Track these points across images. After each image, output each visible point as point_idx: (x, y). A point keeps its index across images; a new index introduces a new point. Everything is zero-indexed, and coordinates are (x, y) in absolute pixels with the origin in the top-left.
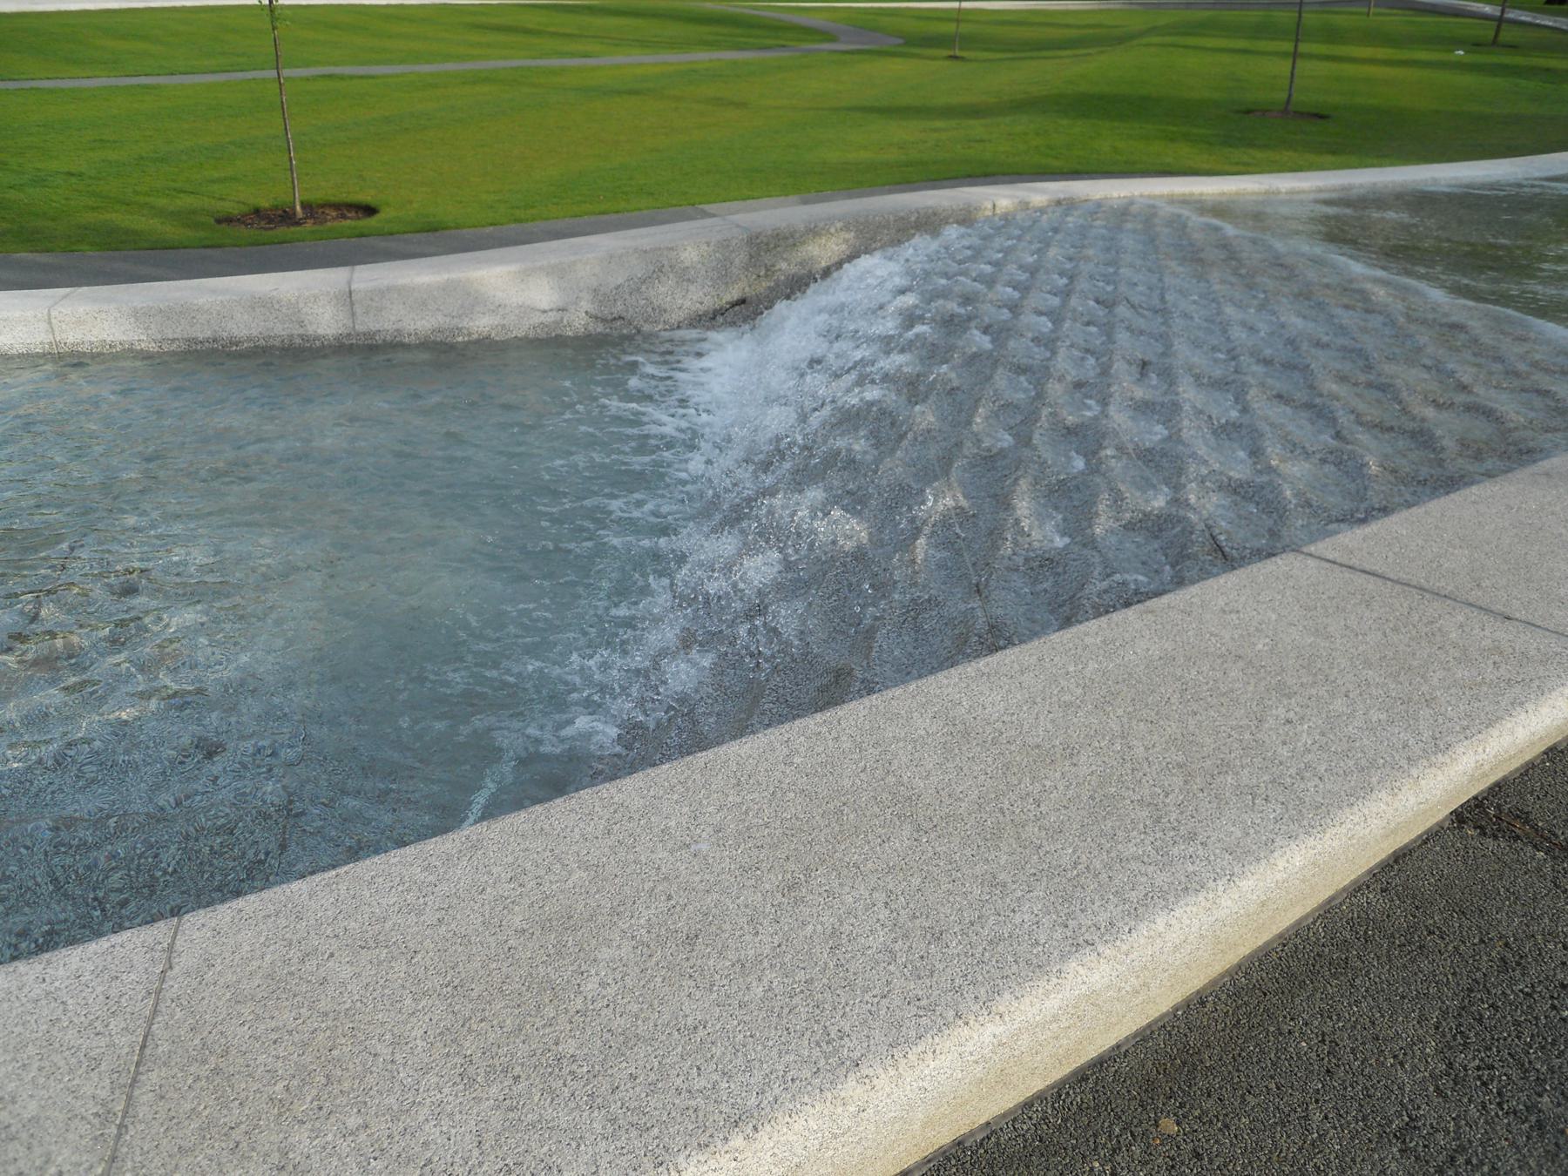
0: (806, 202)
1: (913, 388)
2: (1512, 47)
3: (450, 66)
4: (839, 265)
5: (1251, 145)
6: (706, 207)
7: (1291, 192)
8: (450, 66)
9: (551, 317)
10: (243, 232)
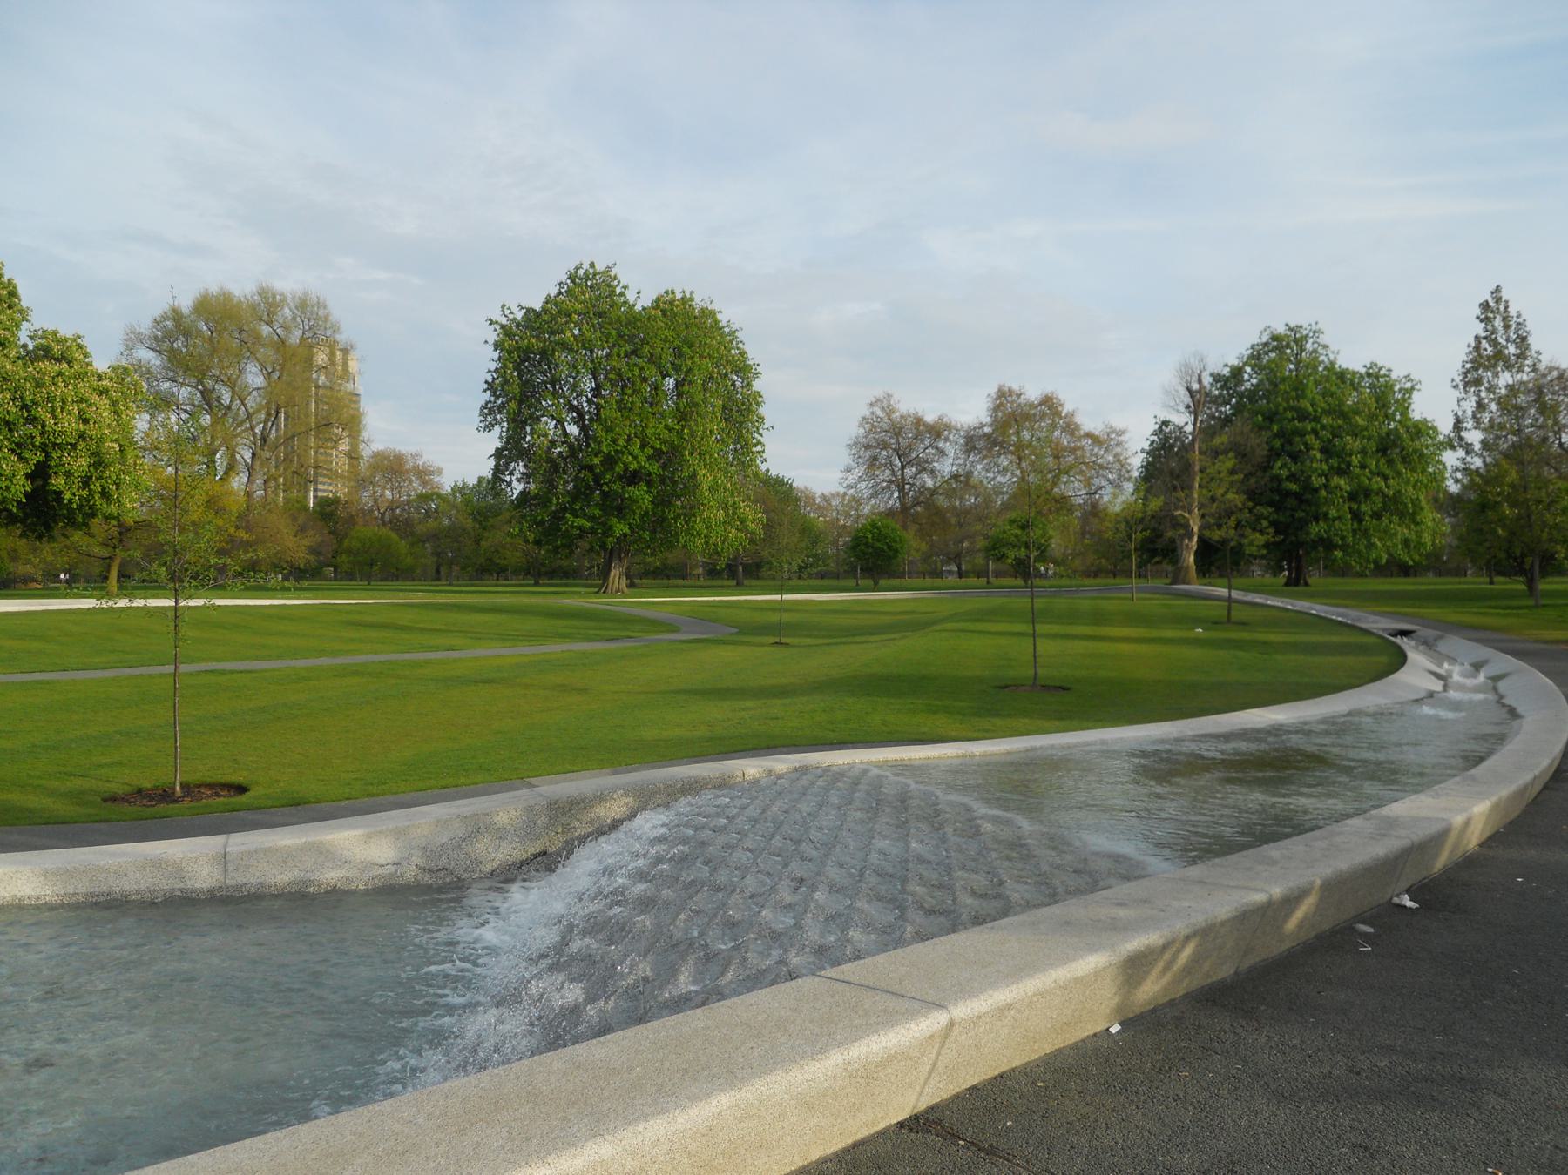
0: (615, 773)
1: (645, 904)
2: (1243, 624)
3: (324, 661)
4: (621, 821)
5: (997, 715)
6: (533, 780)
7: (984, 755)
8: (324, 661)
9: (389, 869)
10: (126, 808)
